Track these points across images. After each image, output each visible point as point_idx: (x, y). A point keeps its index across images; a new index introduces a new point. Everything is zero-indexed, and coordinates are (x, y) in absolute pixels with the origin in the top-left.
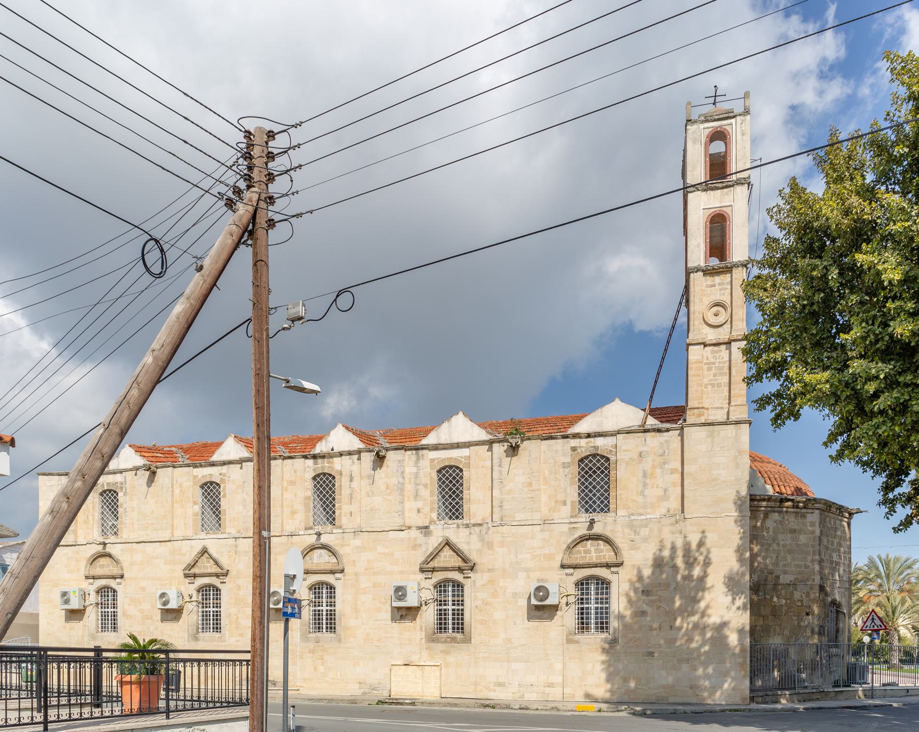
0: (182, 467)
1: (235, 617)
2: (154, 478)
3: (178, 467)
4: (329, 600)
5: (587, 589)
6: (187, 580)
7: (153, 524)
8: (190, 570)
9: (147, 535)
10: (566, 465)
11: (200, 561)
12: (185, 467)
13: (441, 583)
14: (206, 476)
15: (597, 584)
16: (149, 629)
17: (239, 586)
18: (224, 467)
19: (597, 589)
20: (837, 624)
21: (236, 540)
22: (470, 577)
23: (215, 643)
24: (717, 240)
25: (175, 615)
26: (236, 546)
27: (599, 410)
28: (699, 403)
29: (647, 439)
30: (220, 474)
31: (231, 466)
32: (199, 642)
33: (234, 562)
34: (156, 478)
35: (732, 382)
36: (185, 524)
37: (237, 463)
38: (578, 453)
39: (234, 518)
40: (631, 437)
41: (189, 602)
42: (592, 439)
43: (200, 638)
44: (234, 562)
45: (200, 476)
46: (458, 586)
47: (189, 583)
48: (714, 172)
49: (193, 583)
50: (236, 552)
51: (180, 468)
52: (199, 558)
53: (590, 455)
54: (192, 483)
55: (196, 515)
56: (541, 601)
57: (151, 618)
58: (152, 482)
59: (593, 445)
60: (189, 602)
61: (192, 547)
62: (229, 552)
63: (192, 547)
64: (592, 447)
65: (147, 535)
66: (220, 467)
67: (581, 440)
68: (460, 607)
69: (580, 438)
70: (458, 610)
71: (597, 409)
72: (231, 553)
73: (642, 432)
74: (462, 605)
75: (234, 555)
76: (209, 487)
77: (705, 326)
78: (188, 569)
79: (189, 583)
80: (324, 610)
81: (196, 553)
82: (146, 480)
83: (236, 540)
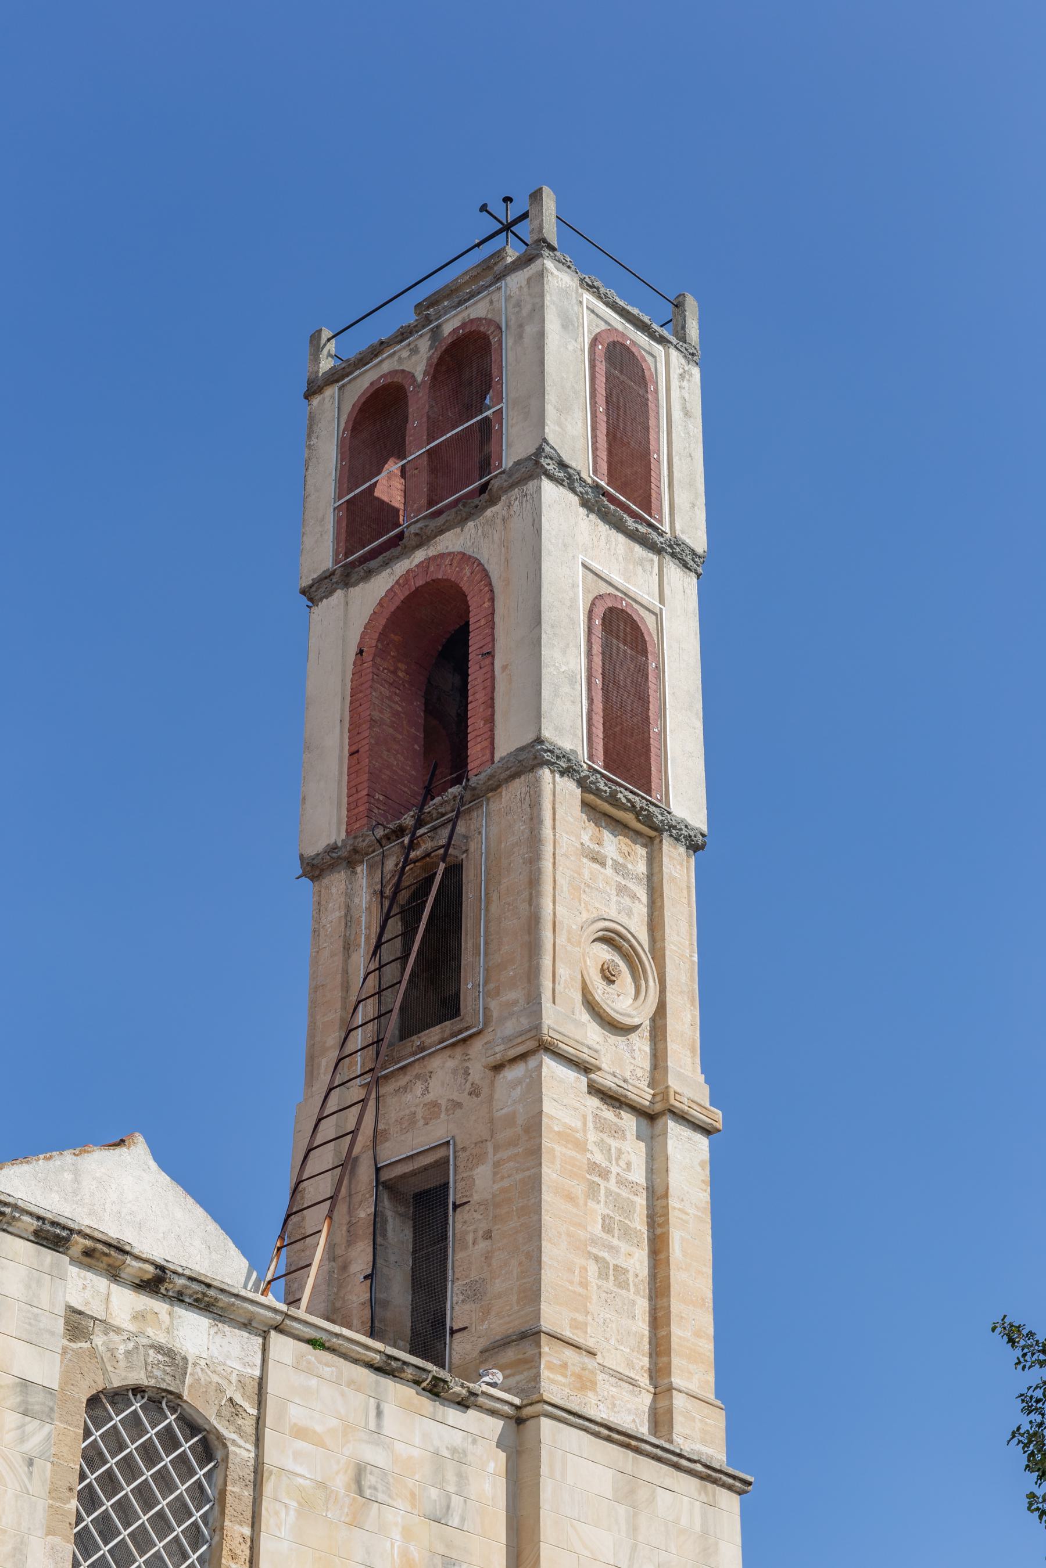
4: (196, 1377)
10: (37, 1399)
20: (445, 297)
24: (640, 324)
27: (68, 1157)
28: (575, 1325)
29: (386, 1408)
35: (600, 581)
38: (93, 1351)
40: (327, 1371)
42: (160, 1307)
48: (667, 1274)
53: (138, 1390)
59: (162, 1339)
64: (159, 1349)
67: (114, 1287)
69: (114, 1275)
71: (61, 1148)
73: (370, 1366)
77: (585, 1017)
80: (139, 1404)
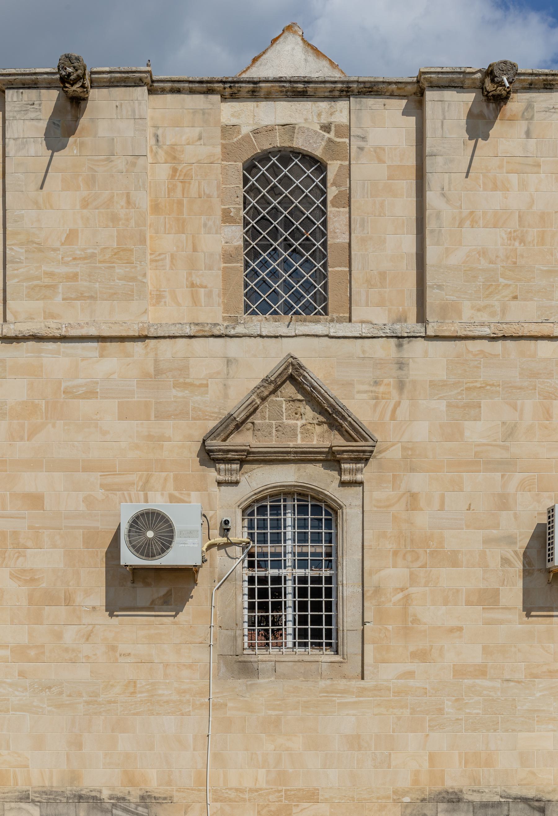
0: (178, 91)
1: (400, 596)
2: (77, 119)
3: (163, 91)
5: (277, 524)
6: (212, 474)
7: (74, 277)
8: (224, 440)
9: (52, 316)
11: (266, 409)
12: (192, 92)
13: (264, 498)
14: (270, 129)
15: (302, 509)
16: (59, 636)
17: (413, 496)
18: (342, 105)
19: (303, 524)
21: (400, 346)
22: (361, 483)
23: (323, 684)
25: (163, 591)
26: (401, 365)
30: (326, 128)
31: (370, 102)
32: (261, 681)
33: (393, 417)
34: (84, 121)
36: (193, 285)
37: (392, 95)
39: (383, 275)
41: (220, 547)
43: (261, 666)
44: (393, 417)
45: (245, 130)
46: (317, 509)
47: (220, 483)
49: (237, 483)
50: (401, 385)
51: (169, 97)
52: (264, 399)
54: (218, 150)
55: (228, 257)
56: (151, 555)
57: (68, 601)
58: (70, 131)
60: (220, 547)
61: (229, 362)
62: (376, 383)
63: (229, 362)
65: (52, 316)
66: (324, 105)
68: (325, 573)
70: (317, 580)
72: (382, 389)
74: (329, 564)
75: (394, 393)
76: (275, 171)
78: (223, 436)
79: (220, 483)
81: (257, 382)
82: (43, 125)
83: (400, 346)
